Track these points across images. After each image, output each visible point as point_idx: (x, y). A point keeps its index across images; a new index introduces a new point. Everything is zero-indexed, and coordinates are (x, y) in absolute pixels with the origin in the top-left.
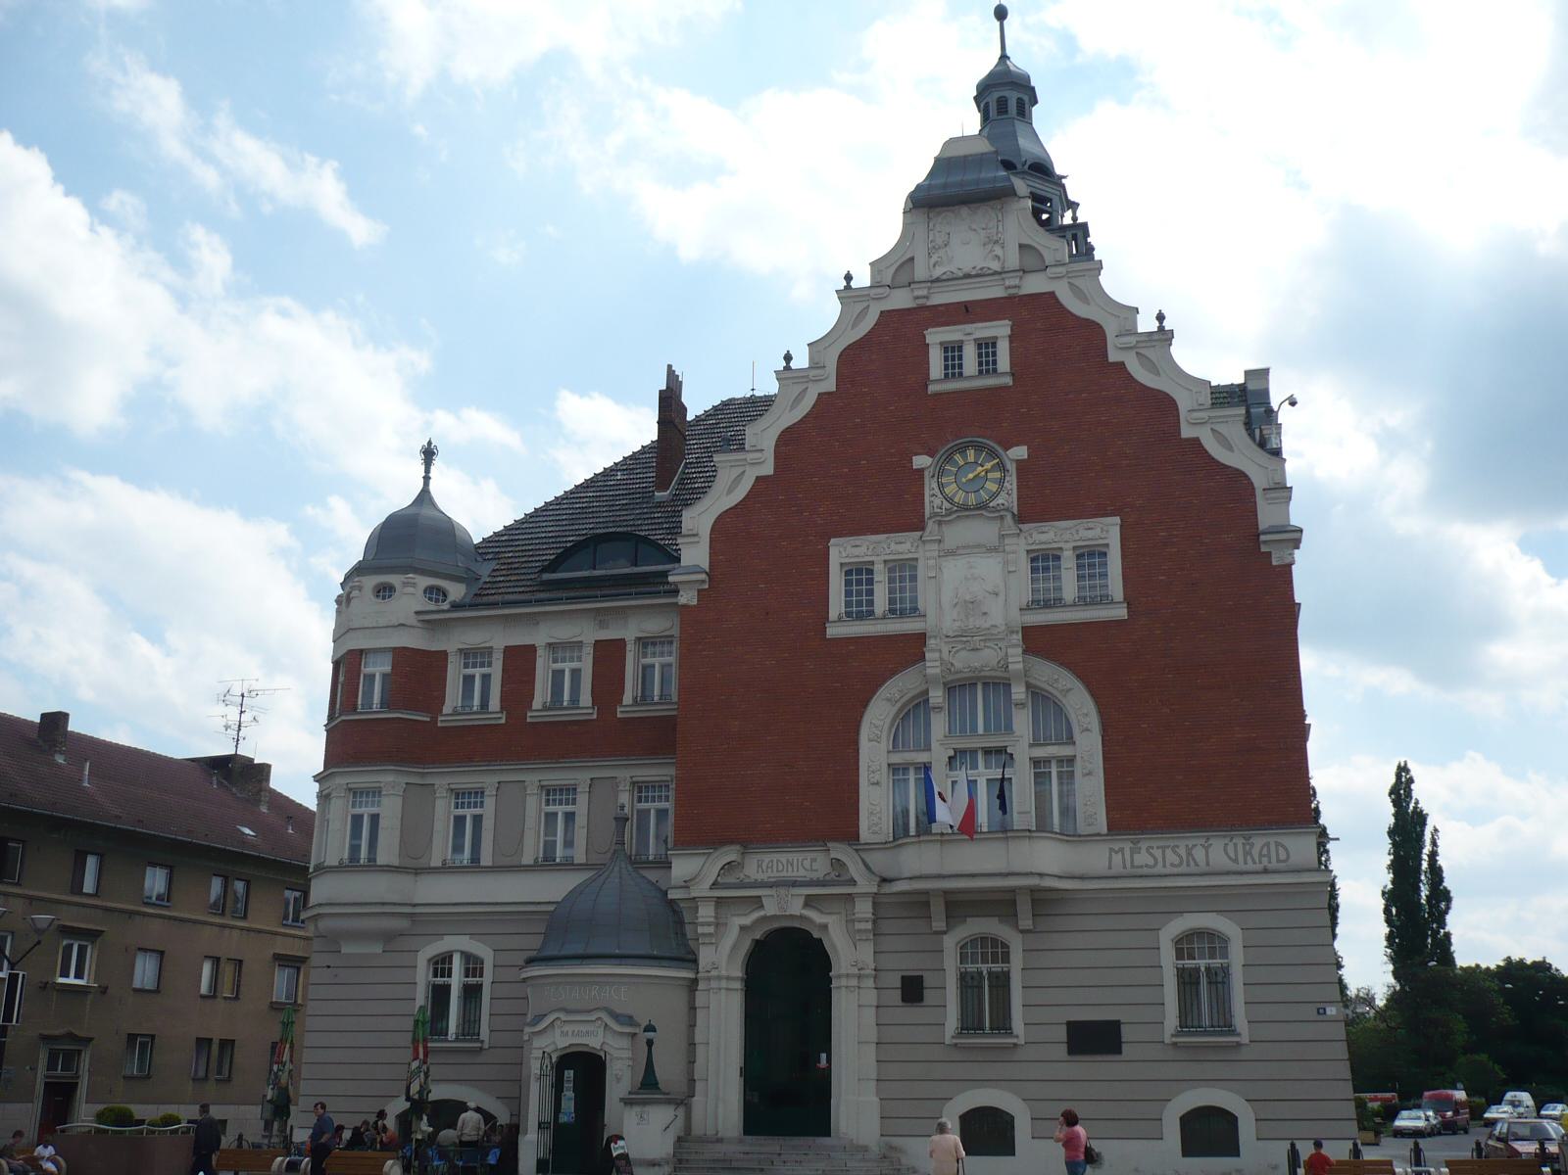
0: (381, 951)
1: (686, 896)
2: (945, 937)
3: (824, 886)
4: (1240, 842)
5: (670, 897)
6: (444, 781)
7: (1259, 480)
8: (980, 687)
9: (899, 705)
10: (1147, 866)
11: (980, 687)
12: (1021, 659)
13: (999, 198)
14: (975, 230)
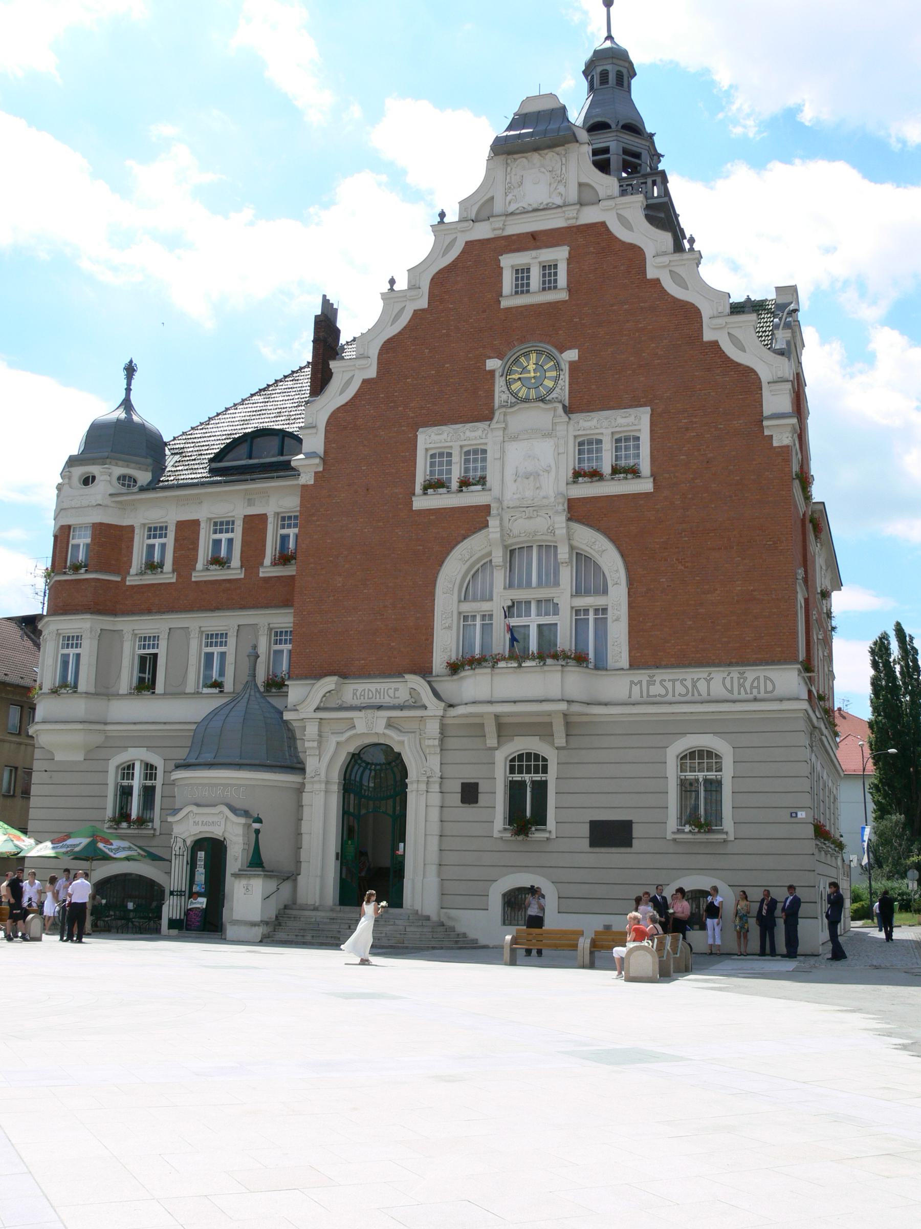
0: (83, 759)
2: (496, 751)
9: (468, 564)
10: (660, 695)
12: (564, 525)
14: (543, 173)
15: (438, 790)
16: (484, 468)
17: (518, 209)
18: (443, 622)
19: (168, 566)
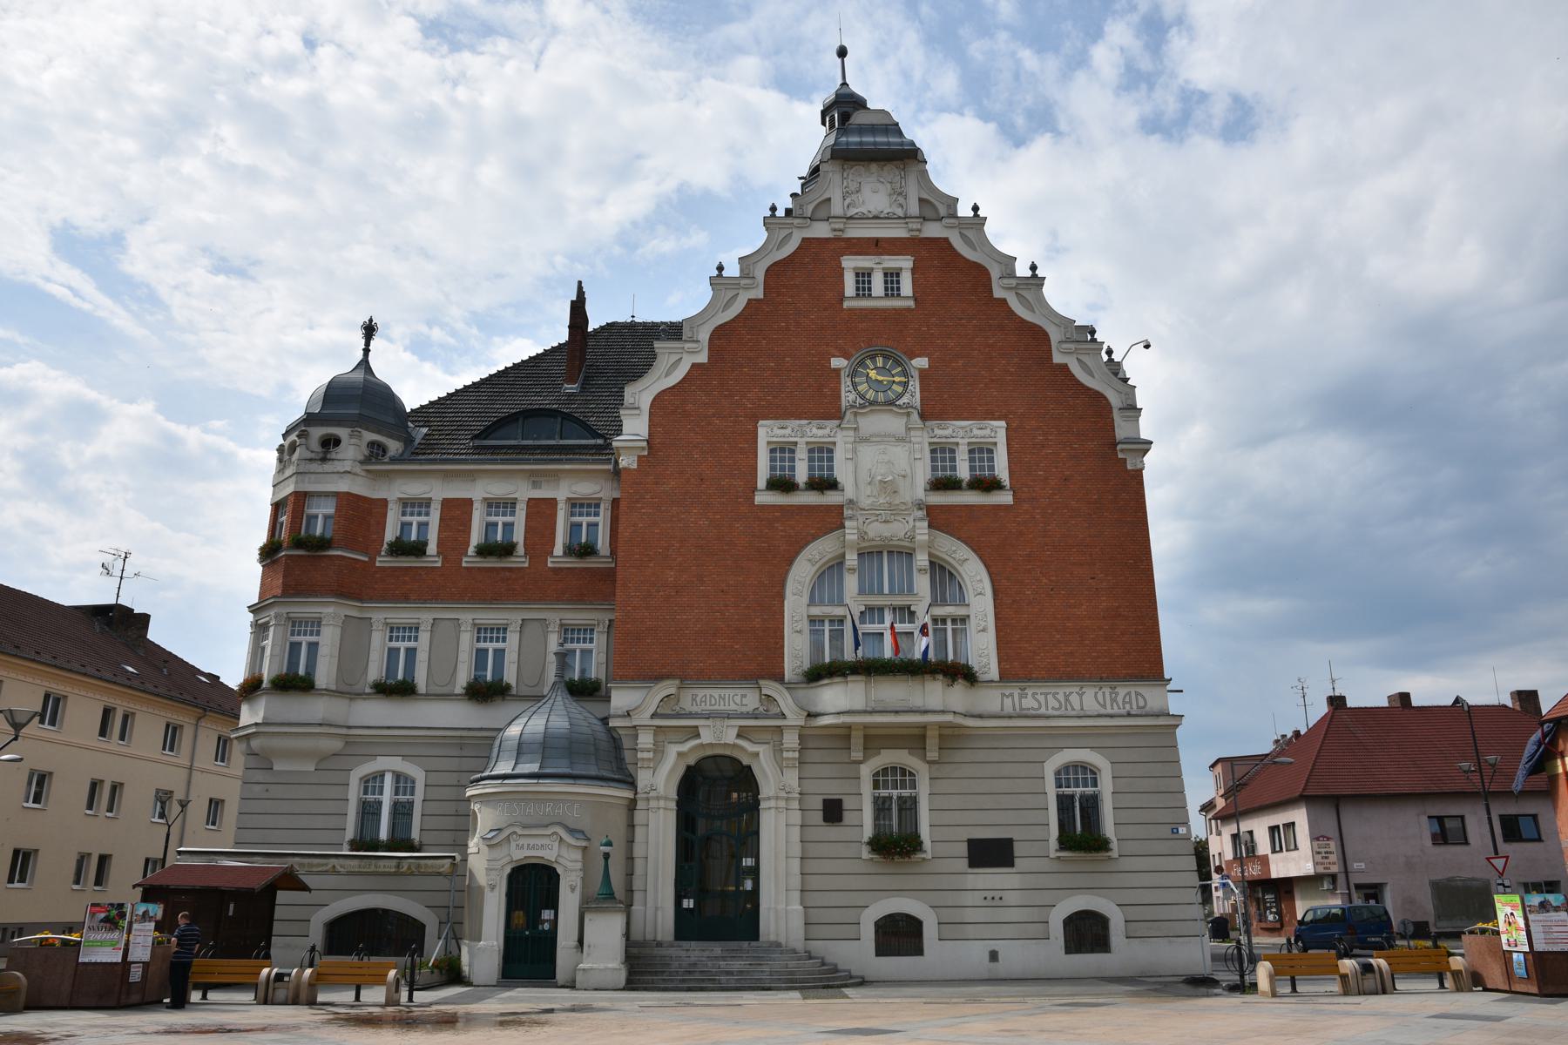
0: (313, 769)
1: (630, 725)
3: (756, 718)
4: (1107, 691)
5: (610, 725)
6: (381, 615)
7: (1114, 399)
8: (885, 554)
11: (885, 554)
13: (901, 159)
14: (883, 183)
15: (798, 807)
16: (831, 468)
17: (857, 214)
18: (794, 625)
19: (521, 550)
